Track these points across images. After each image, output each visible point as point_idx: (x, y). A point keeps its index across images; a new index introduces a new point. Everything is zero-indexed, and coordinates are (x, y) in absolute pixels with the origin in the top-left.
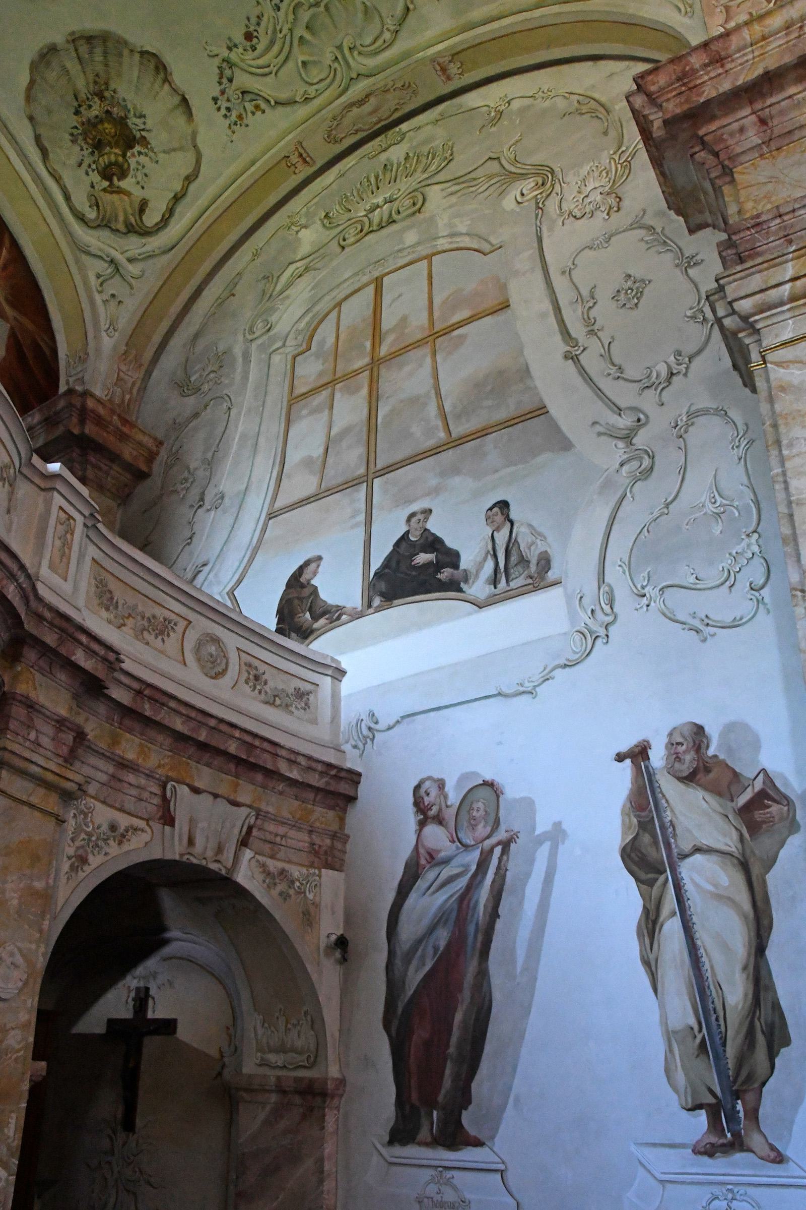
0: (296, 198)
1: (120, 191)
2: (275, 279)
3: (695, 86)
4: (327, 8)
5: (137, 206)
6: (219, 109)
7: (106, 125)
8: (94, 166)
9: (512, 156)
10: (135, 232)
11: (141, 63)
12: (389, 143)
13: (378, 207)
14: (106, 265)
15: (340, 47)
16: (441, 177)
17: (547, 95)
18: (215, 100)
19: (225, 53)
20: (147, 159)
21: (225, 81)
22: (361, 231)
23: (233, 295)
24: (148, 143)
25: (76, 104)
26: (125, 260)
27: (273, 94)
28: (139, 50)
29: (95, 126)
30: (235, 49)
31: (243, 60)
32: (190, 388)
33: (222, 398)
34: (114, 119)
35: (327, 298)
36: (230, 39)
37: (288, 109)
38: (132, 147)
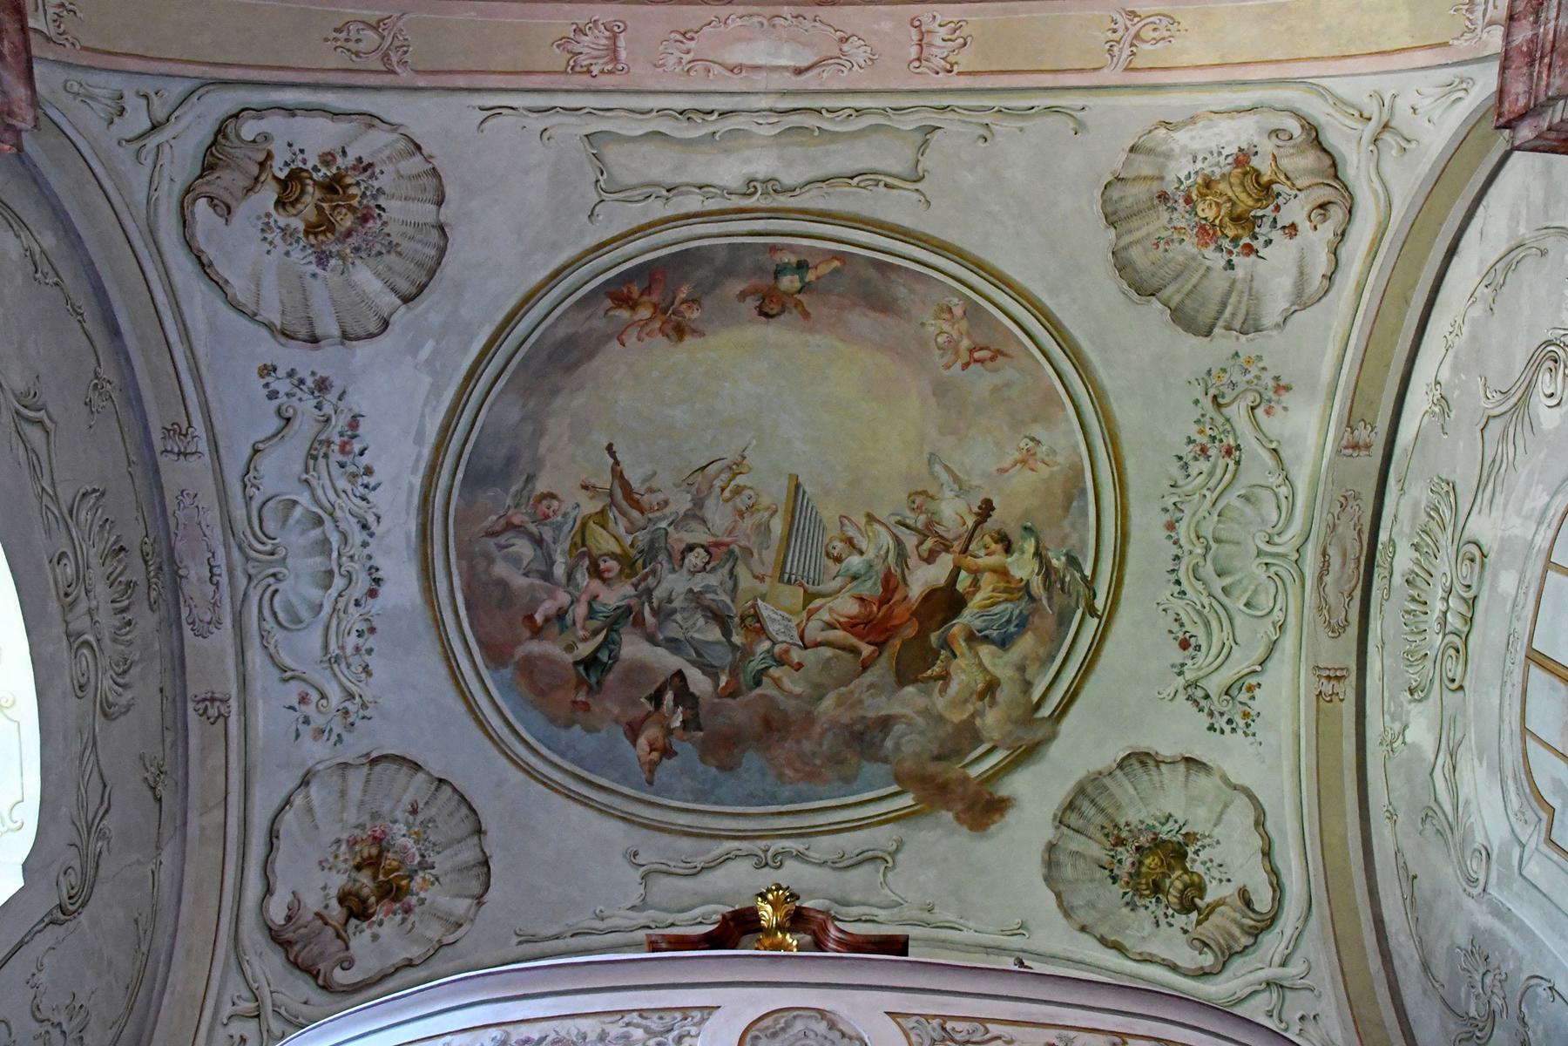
0: (1368, 720)
1: (1212, 908)
2: (1436, 808)
3: (1554, 42)
4: (1217, 540)
5: (1239, 903)
6: (1222, 732)
7: (1147, 861)
8: (1170, 911)
9: (1498, 396)
10: (1262, 930)
11: (1126, 775)
12: (1387, 565)
13: (1445, 613)
14: (1267, 994)
15: (1260, 553)
16: (1464, 507)
17: (1456, 329)
18: (1211, 728)
19: (1181, 681)
20: (1207, 849)
21: (1203, 703)
22: (1458, 651)
23: (1415, 877)
24: (1195, 834)
25: (1107, 873)
26: (1281, 970)
27: (1251, 662)
28: (1115, 765)
29: (1138, 874)
30: (1185, 668)
31: (1200, 669)
32: (1481, 1025)
33: (1528, 988)
34: (1150, 848)
35: (1506, 744)
36: (1173, 666)
37: (1276, 655)
38: (1185, 855)
